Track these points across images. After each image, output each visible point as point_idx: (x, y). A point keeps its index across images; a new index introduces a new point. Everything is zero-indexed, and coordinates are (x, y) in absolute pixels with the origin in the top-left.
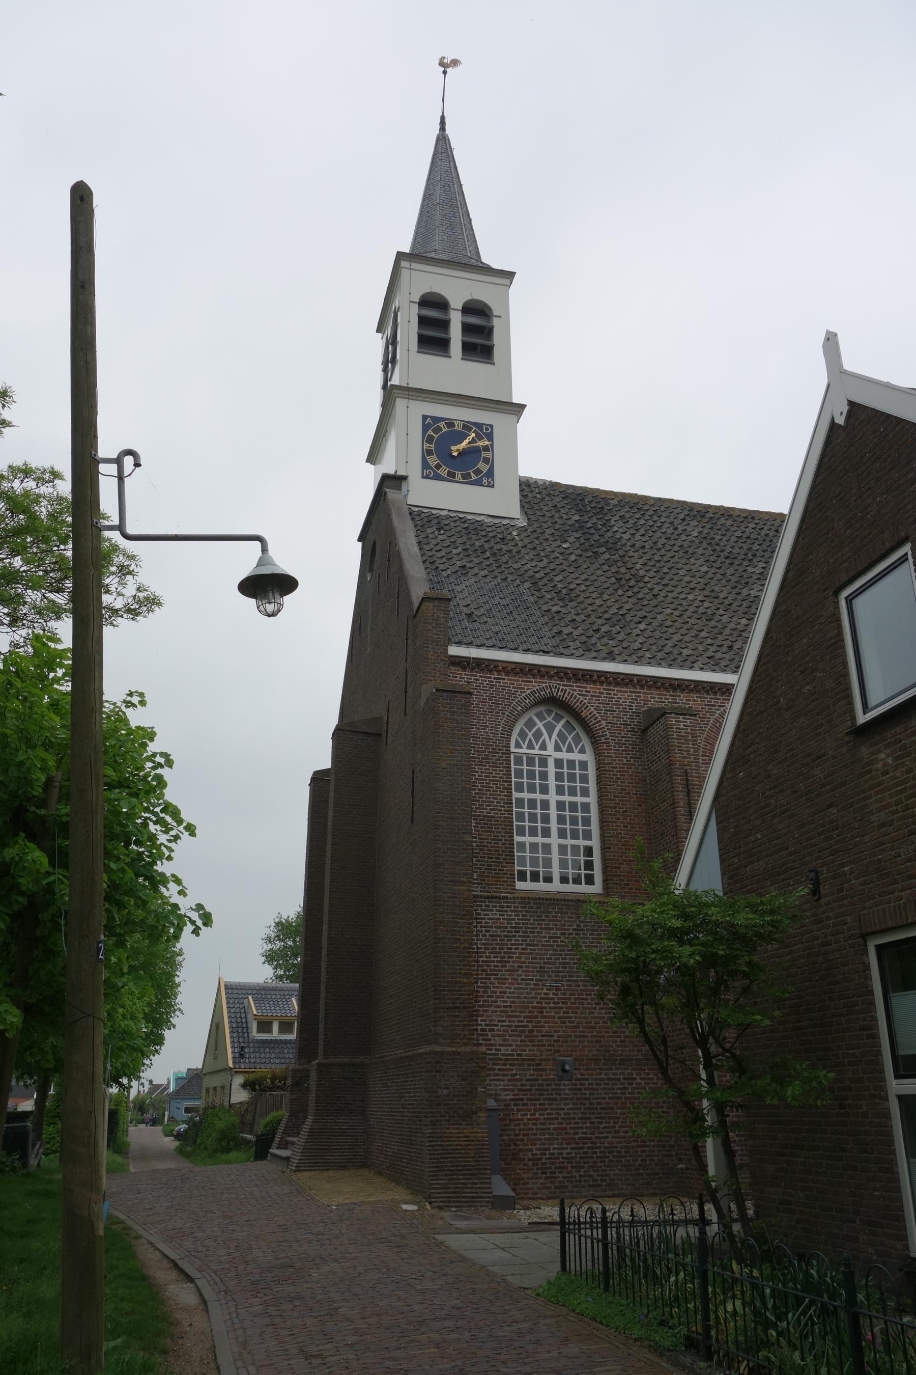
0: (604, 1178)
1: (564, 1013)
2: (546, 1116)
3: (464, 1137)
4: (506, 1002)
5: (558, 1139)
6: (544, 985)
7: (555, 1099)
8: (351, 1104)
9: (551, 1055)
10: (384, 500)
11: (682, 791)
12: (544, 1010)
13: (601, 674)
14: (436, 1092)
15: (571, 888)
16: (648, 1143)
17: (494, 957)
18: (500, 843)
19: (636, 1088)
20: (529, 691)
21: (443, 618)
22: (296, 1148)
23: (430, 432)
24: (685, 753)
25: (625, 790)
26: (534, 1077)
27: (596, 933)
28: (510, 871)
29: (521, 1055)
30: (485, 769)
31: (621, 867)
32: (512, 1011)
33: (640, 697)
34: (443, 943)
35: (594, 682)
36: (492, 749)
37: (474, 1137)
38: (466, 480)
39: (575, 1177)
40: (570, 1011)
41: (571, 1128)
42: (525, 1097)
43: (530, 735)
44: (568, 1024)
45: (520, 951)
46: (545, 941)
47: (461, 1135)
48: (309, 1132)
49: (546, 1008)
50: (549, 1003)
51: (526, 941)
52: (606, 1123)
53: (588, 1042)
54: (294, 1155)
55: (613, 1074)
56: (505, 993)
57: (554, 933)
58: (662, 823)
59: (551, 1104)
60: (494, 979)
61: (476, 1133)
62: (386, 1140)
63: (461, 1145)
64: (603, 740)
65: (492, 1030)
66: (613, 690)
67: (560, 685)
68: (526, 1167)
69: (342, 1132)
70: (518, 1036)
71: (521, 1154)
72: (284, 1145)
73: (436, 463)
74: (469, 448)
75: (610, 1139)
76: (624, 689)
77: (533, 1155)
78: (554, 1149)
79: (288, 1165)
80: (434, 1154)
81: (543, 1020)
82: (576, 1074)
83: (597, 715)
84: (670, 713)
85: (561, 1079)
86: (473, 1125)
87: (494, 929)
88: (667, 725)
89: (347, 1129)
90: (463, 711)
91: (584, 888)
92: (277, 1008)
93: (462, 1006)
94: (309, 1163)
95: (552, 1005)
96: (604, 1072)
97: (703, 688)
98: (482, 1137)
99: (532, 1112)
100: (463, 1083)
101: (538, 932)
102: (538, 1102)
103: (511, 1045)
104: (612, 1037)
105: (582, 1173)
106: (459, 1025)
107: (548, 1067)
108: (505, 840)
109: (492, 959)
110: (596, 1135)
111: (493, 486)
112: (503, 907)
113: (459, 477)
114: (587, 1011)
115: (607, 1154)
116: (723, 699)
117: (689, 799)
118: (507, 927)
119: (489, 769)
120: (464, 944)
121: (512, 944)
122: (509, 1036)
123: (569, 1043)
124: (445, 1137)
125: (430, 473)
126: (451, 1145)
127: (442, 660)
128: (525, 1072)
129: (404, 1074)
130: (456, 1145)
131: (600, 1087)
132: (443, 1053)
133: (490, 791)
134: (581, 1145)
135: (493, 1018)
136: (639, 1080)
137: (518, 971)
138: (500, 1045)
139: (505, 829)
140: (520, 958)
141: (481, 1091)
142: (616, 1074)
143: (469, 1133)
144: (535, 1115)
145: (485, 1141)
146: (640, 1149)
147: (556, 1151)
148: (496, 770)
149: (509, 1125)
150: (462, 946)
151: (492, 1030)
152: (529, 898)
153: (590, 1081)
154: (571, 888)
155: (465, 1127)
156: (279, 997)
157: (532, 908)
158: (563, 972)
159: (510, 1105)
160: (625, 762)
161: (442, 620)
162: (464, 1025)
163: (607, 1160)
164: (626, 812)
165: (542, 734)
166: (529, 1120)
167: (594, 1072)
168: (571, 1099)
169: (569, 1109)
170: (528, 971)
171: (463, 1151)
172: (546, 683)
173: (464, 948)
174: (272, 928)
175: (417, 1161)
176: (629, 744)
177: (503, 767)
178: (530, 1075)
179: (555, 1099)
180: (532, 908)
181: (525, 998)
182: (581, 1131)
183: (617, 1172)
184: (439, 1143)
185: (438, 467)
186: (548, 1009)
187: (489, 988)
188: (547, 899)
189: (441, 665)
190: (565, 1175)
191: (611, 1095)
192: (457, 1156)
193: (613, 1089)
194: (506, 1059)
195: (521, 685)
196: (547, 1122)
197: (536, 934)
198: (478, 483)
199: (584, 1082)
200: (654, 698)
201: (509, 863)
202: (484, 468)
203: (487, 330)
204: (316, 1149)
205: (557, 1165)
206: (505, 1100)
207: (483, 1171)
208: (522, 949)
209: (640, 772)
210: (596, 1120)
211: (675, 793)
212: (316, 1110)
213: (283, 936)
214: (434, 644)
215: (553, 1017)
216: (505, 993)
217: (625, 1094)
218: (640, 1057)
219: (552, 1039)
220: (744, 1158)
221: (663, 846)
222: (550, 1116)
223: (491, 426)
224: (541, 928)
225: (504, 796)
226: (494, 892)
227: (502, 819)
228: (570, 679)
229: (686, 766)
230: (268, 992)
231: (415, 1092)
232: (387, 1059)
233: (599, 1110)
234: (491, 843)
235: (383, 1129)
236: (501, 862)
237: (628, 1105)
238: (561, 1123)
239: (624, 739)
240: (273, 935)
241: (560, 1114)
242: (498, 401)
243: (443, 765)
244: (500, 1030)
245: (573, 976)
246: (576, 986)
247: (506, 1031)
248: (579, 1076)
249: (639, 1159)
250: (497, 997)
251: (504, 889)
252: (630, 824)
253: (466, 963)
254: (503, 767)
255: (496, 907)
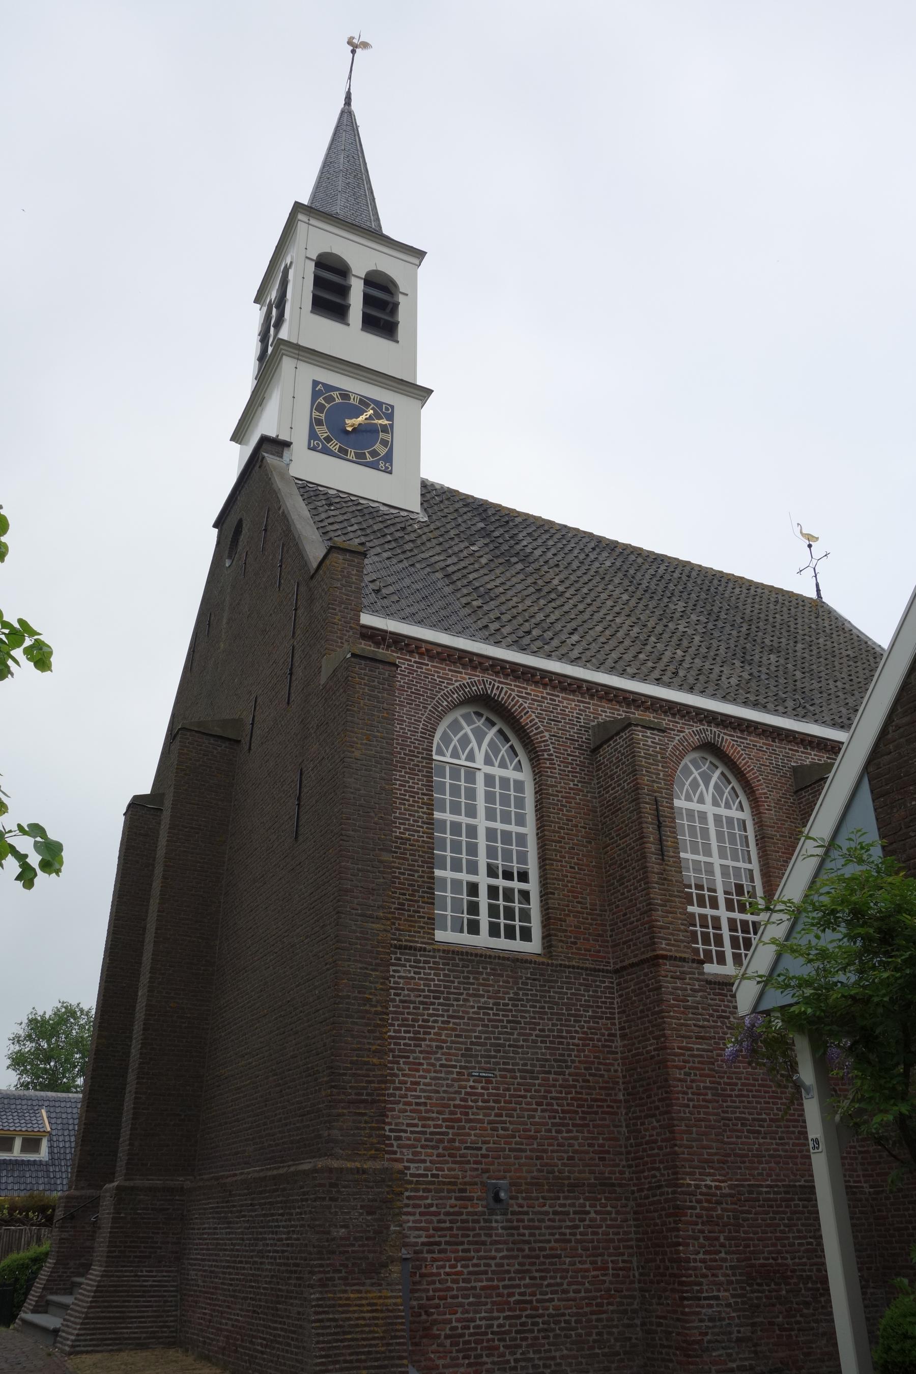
0: (548, 1362)
1: (496, 1115)
2: (471, 1269)
3: (369, 1305)
4: (419, 1097)
5: (486, 1304)
6: (470, 1075)
7: (484, 1243)
8: (160, 1248)
9: (477, 1176)
10: (260, 467)
11: (652, 824)
12: (470, 1111)
13: (545, 673)
14: (329, 1233)
15: (502, 943)
16: (605, 1308)
17: (405, 1032)
18: (416, 875)
19: (589, 1226)
20: (457, 684)
21: (356, 575)
22: (71, 1316)
23: (321, 400)
24: (654, 776)
25: (572, 821)
26: (456, 1209)
27: (538, 1005)
28: (428, 913)
29: (437, 1176)
30: (400, 776)
31: (568, 919)
32: (427, 1111)
33: (589, 708)
34: (347, 1003)
35: (536, 683)
36: (410, 751)
37: (383, 1304)
38: (360, 460)
39: (508, 1362)
40: (504, 1113)
41: (505, 1287)
42: (443, 1240)
43: (455, 740)
44: (501, 1132)
45: (440, 1024)
46: (474, 1013)
47: (364, 1302)
48: (95, 1292)
49: (472, 1107)
50: (476, 1101)
51: (448, 1011)
52: (551, 1278)
53: (526, 1158)
54: (67, 1326)
55: (561, 1205)
56: (418, 1083)
57: (485, 1003)
58: (621, 864)
59: (478, 1251)
60: (405, 1063)
61: (386, 1298)
62: (220, 1306)
63: (364, 1319)
64: (546, 756)
65: (398, 1138)
66: (558, 696)
67: (495, 681)
68: (441, 1349)
69: (144, 1291)
70: (433, 1147)
71: (435, 1328)
72: (42, 1307)
73: (326, 435)
74: (365, 424)
75: (556, 1303)
76: (571, 697)
77: (452, 1329)
78: (481, 1319)
79: (55, 1342)
80: (323, 1335)
81: (468, 1125)
82: (512, 1206)
83: (539, 724)
84: (637, 725)
85: (492, 1212)
86: (380, 1285)
87: (406, 992)
88: (632, 739)
89: (152, 1286)
90: (386, 686)
91: (517, 945)
92: (23, 1121)
93: (369, 1098)
94: (91, 1340)
95: (480, 1104)
96: (548, 1202)
97: (661, 707)
98: (395, 1304)
99: (453, 1262)
100: (369, 1218)
101: (465, 1000)
102: (460, 1248)
103: (424, 1161)
104: (557, 1151)
105: (518, 1356)
106: (365, 1128)
107: (475, 1195)
108: (423, 872)
109: (403, 1034)
110: (538, 1297)
111: (390, 473)
112: (419, 961)
113: (351, 455)
114: (526, 1113)
115: (552, 1325)
116: (683, 724)
117: (660, 833)
118: (423, 991)
119: (404, 777)
120: (376, 1006)
121: (429, 1015)
122: (423, 1147)
123: (502, 1160)
124: (340, 1306)
125: (316, 444)
126: (349, 1319)
127: (351, 628)
128: (444, 1201)
129: (265, 1204)
130: (358, 1319)
131: (543, 1225)
132: (341, 1170)
133: (404, 804)
134: (518, 1313)
135: (400, 1121)
136: (593, 1215)
137: (436, 1053)
138: (409, 1161)
139: (423, 857)
140: (440, 1035)
141: (395, 1232)
142: (564, 1205)
143: (375, 1298)
144: (455, 1266)
145: (399, 1311)
146: (594, 1317)
147: (483, 1323)
148: (414, 779)
149: (419, 1283)
150: (373, 1009)
151: (398, 1138)
152: (453, 952)
153: (531, 1216)
154: (502, 943)
155: (369, 1288)
156: (25, 1107)
157: (457, 965)
158: (495, 1057)
159: (422, 1253)
160: (572, 786)
161: (354, 577)
162: (371, 1128)
163: (551, 1335)
164: (574, 849)
165: (469, 742)
166: (448, 1274)
167: (536, 1202)
168: (505, 1242)
169: (502, 1258)
170: (449, 1054)
171: (367, 1329)
172: (478, 676)
173: (376, 1013)
174: (23, 1025)
175: (289, 1345)
176: (577, 765)
177: (423, 776)
178: (451, 1207)
179: (484, 1243)
180: (457, 965)
181: (445, 1092)
182: (518, 1290)
183: (565, 1352)
184: (331, 1316)
185: (328, 439)
186: (475, 1110)
187: (397, 1076)
188: (476, 955)
189: (351, 633)
190: (496, 1359)
191: (557, 1236)
192: (359, 1336)
193: (561, 1228)
194: (418, 1183)
195: (447, 674)
196: (473, 1277)
197: (461, 1003)
198: (373, 466)
199: (522, 1217)
200: (606, 712)
201: (427, 903)
202: (383, 451)
203: (390, 306)
204: (105, 1318)
205: (485, 1344)
206: (416, 1244)
207: (397, 1362)
208: (443, 1022)
209: (588, 801)
210: (537, 1275)
211: (644, 825)
212: (108, 1257)
213: (36, 1036)
214: (343, 606)
215: (480, 1121)
216: (418, 1083)
217: (574, 1234)
218: (592, 1181)
219: (479, 1153)
220: (742, 1329)
221: (623, 894)
222: (476, 1269)
224: (468, 994)
225: (424, 813)
226: (406, 941)
227: (420, 844)
228: (508, 675)
229: (656, 792)
230: (13, 1101)
231: (288, 1233)
232: (229, 1180)
233: (542, 1259)
234: (404, 874)
235: (216, 1288)
236: (418, 901)
237: (580, 1251)
238: (492, 1280)
239: (570, 758)
240: (22, 1033)
241: (490, 1265)
242: (402, 380)
243: (357, 754)
244: (409, 1139)
245: (508, 1064)
246: (512, 1077)
247: (419, 1140)
248: (516, 1209)
249: (594, 1331)
250: (407, 1089)
251: (419, 937)
252: (578, 864)
253: (378, 1034)
254: (423, 776)
255: (409, 961)
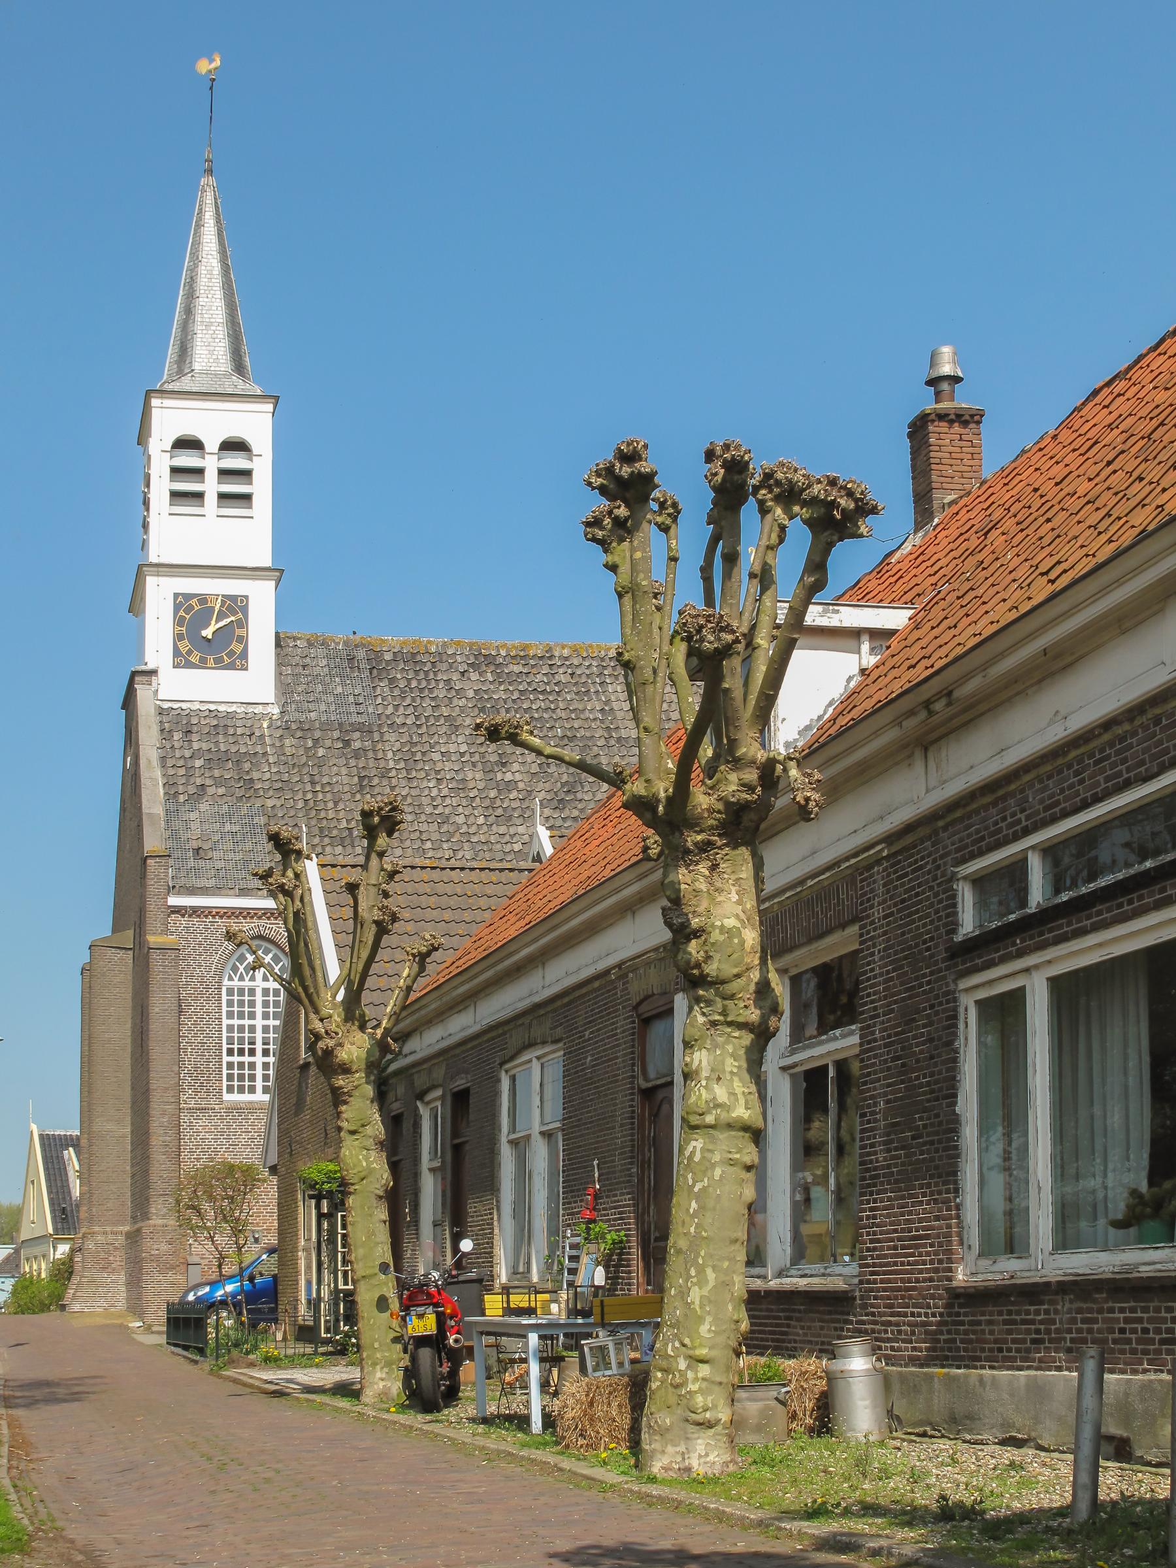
23: (181, 613)
38: (220, 665)
113: (211, 663)
125: (181, 660)
185: (189, 652)
198: (231, 667)
223: (247, 597)
